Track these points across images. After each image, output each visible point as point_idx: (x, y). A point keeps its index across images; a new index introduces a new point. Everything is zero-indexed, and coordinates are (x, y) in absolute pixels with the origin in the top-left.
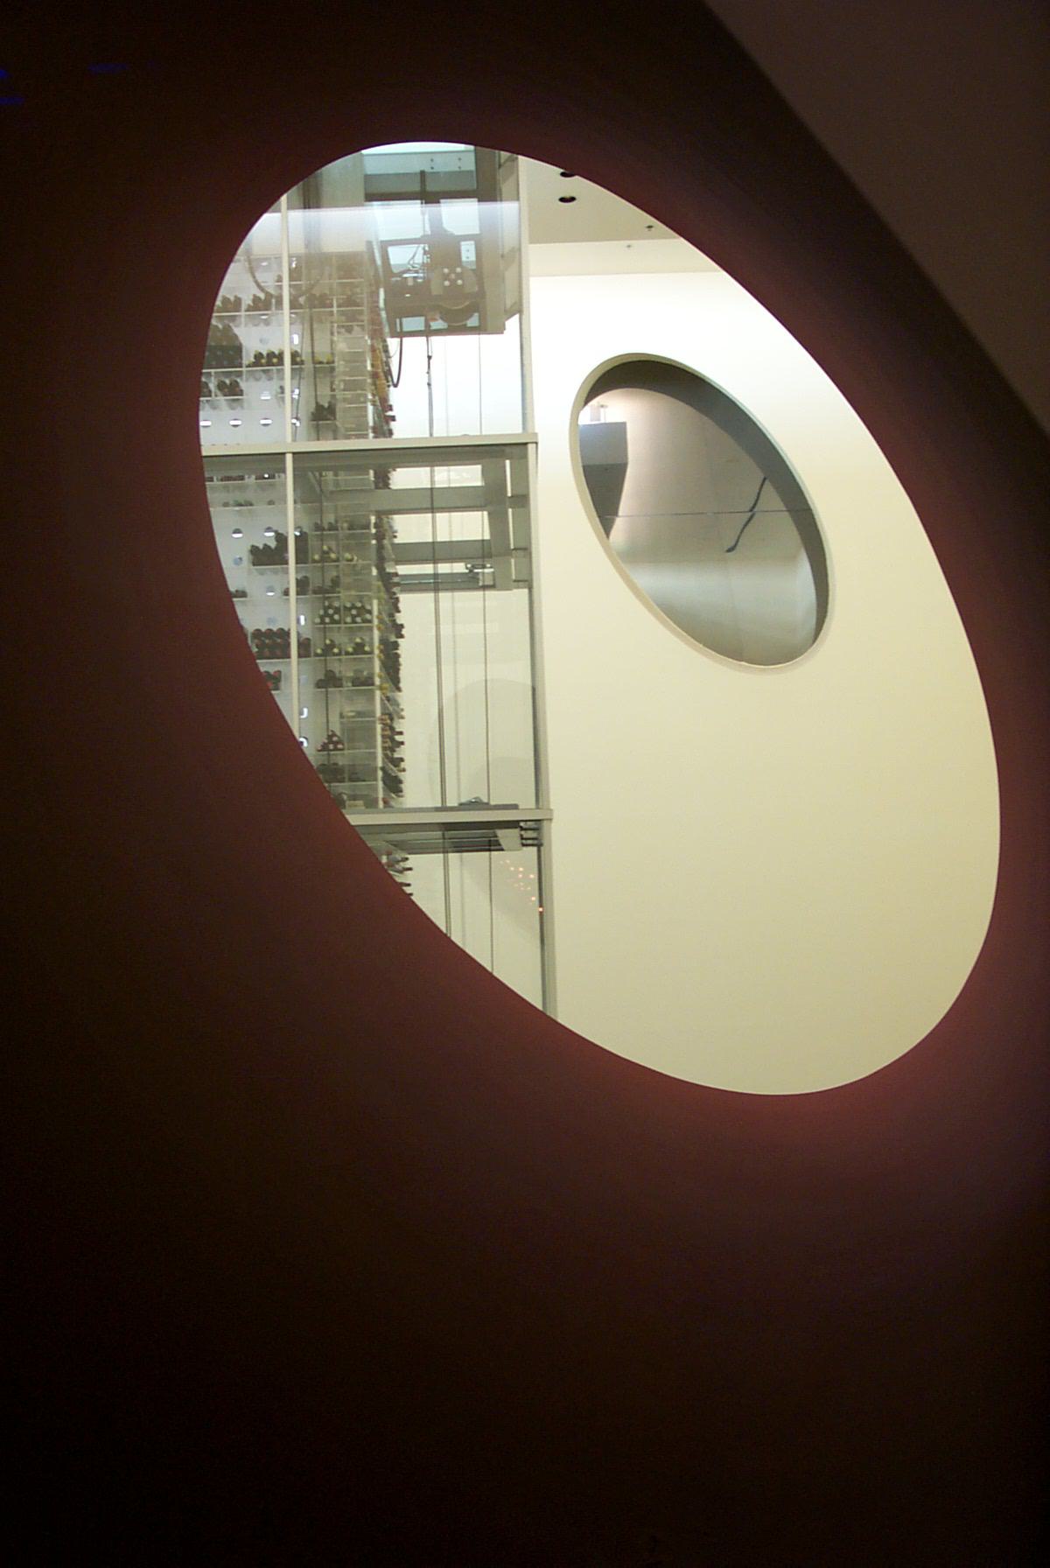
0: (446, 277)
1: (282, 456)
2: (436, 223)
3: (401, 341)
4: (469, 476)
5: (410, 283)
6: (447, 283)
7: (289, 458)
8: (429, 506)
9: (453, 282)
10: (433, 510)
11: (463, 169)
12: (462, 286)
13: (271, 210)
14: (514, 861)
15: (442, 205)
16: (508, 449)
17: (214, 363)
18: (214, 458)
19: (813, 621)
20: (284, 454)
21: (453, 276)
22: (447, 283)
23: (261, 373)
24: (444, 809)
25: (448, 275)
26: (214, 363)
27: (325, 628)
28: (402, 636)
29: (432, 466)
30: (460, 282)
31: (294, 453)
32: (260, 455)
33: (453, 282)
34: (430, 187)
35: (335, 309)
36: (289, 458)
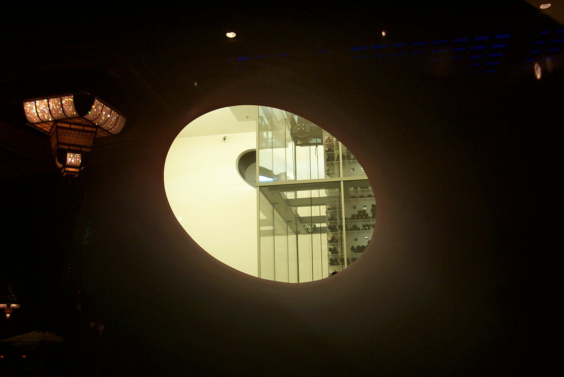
0: (299, 127)
3: (286, 149)
4: (322, 193)
6: (299, 129)
7: (342, 183)
8: (310, 204)
9: (301, 129)
10: (311, 205)
13: (343, 145)
18: (352, 181)
20: (340, 181)
21: (301, 127)
22: (299, 129)
25: (300, 126)
27: (312, 228)
28: (354, 215)
29: (319, 189)
31: (343, 181)
32: (320, 182)
33: (301, 129)
36: (342, 183)
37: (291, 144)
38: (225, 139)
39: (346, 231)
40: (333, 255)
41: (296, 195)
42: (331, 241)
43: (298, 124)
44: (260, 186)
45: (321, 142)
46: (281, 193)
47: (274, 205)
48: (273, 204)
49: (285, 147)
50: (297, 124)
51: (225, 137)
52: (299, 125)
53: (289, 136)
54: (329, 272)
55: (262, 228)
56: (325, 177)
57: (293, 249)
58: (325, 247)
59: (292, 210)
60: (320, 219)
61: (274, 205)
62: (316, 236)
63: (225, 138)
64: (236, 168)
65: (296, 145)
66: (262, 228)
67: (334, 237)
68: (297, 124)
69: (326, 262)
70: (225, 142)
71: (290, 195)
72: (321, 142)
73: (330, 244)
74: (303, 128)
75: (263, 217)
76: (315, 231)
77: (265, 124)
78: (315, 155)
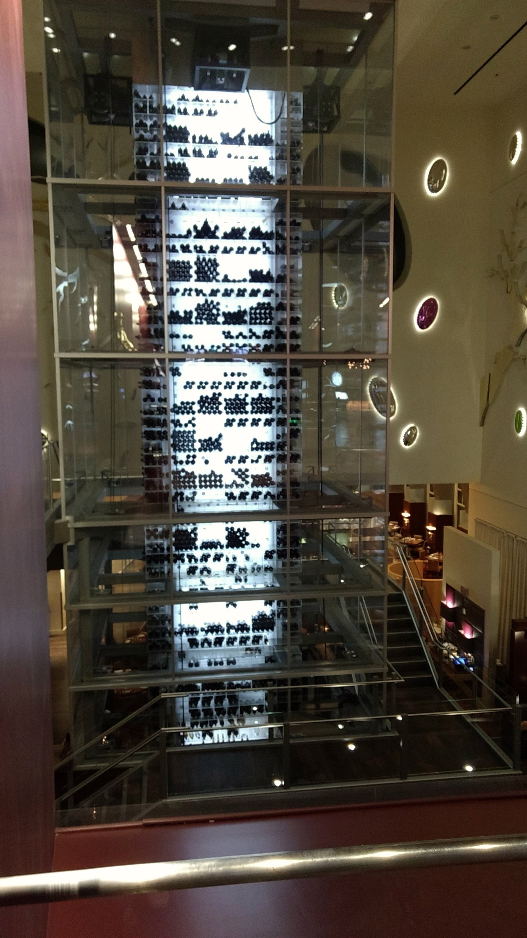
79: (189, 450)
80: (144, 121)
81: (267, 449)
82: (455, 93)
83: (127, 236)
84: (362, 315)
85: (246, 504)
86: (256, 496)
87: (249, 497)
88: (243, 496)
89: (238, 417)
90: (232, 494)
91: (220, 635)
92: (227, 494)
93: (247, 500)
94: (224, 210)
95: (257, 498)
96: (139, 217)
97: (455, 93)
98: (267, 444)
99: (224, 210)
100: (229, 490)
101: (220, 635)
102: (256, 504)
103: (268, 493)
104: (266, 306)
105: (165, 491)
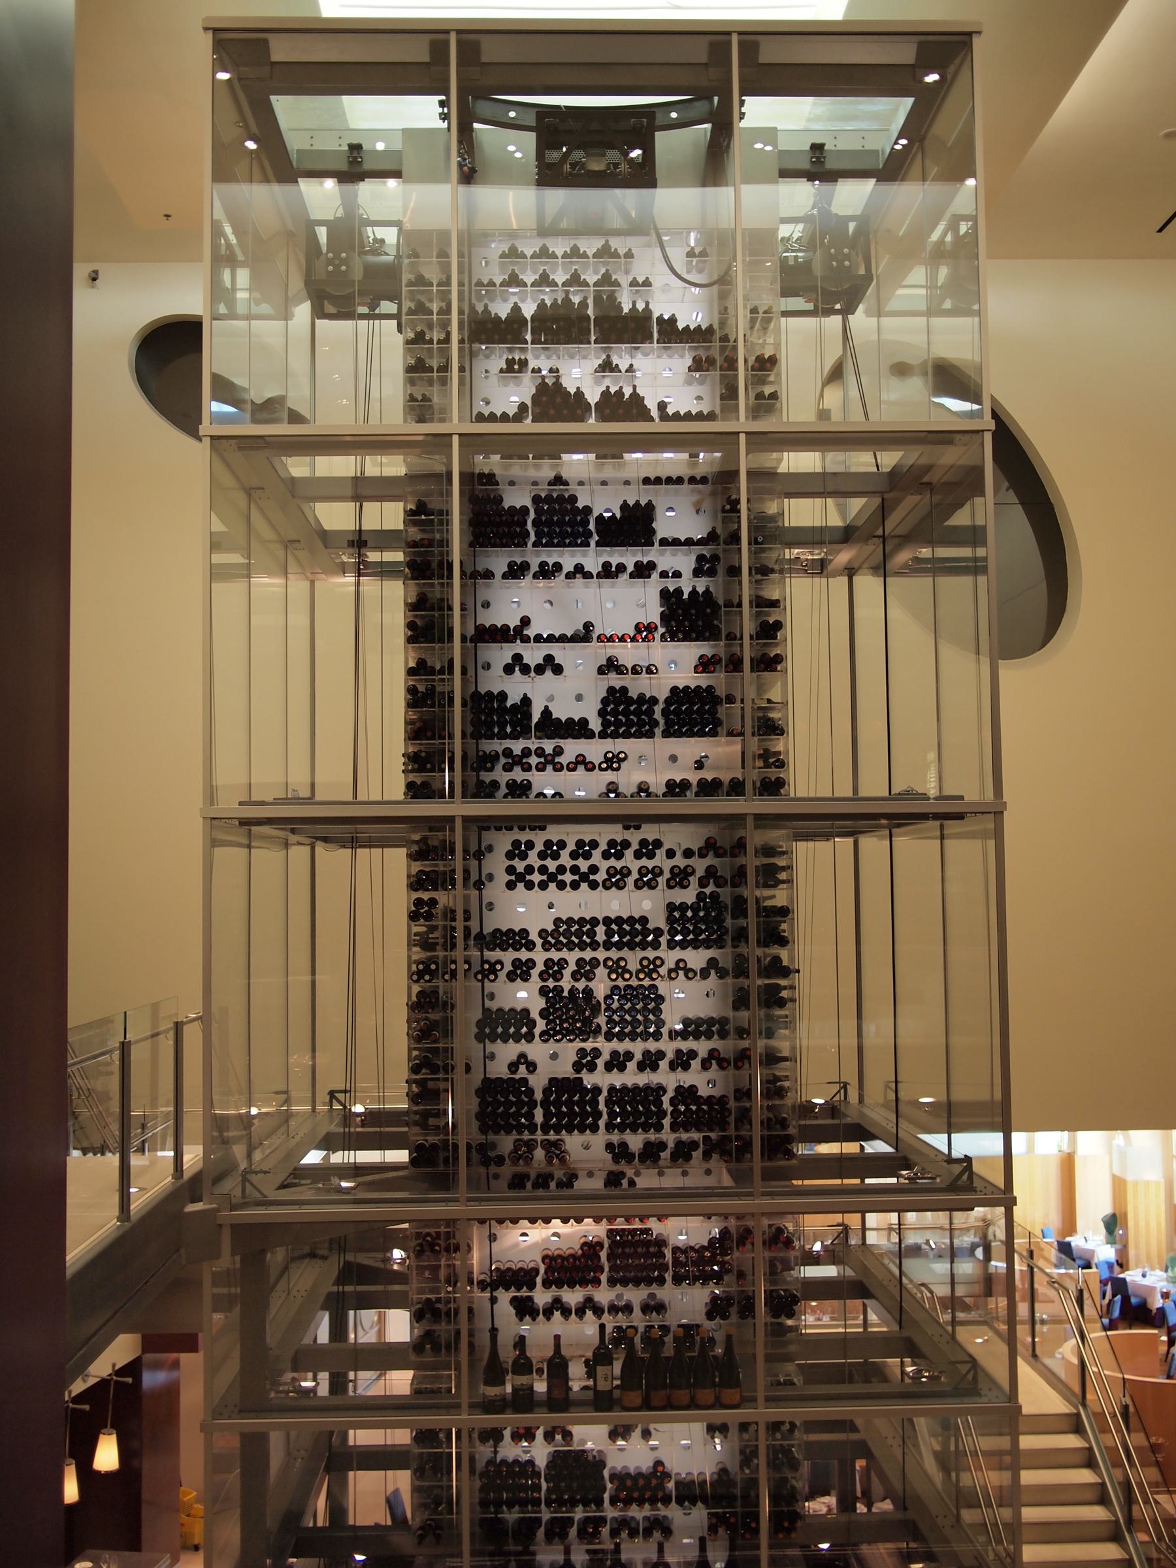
0: (330, 262)
1: (735, 437)
2: (350, 205)
5: (791, 262)
6: (330, 268)
11: (867, 148)
12: (346, 271)
14: (229, 805)
15: (839, 183)
16: (958, 436)
17: (496, 337)
19: (1041, 592)
20: (451, 435)
21: (337, 262)
22: (330, 268)
23: (541, 351)
24: (891, 797)
26: (496, 337)
30: (847, 263)
31: (460, 435)
34: (831, 164)
35: (435, 288)
37: (303, 311)
38: (94, 279)
39: (461, 578)
40: (421, 648)
41: (313, 467)
42: (418, 605)
43: (327, 253)
44: (211, 437)
45: (396, 312)
46: (276, 461)
47: (253, 492)
48: (249, 492)
49: (286, 319)
50: (324, 250)
51: (96, 272)
52: (330, 255)
53: (297, 283)
54: (406, 662)
55: (218, 558)
56: (405, 421)
57: (299, 620)
58: (400, 900)
59: (304, 509)
60: (385, 539)
61: (253, 492)
62: (370, 585)
63: (94, 275)
64: (130, 365)
65: (319, 313)
66: (218, 558)
67: (423, 594)
68: (324, 250)
69: (397, 763)
70: (93, 287)
71: (298, 467)
72: (396, 312)
73: (853, 1428)
74: (343, 268)
75: (218, 526)
76: (363, 567)
77: (229, 245)
78: (342, 6)
79: (520, 1128)
80: (428, 305)
81: (709, 1036)
82: (1160, 230)
83: (380, 548)
84: (411, 206)
85: (661, 1174)
86: (682, 1152)
87: (665, 1155)
88: (651, 1153)
89: (638, 1048)
90: (624, 1145)
91: (524, 955)
92: (609, 1146)
93: (661, 1163)
94: (604, 483)
95: (688, 1157)
96: (412, 506)
97: (1160, 230)
98: (711, 1021)
99: (604, 483)
100: (615, 1138)
101: (524, 955)
102: (685, 1174)
103: (713, 1054)
104: (490, 326)
105: (436, 416)
